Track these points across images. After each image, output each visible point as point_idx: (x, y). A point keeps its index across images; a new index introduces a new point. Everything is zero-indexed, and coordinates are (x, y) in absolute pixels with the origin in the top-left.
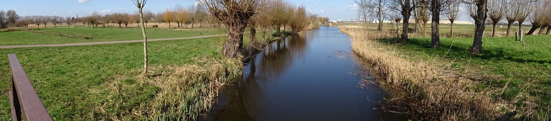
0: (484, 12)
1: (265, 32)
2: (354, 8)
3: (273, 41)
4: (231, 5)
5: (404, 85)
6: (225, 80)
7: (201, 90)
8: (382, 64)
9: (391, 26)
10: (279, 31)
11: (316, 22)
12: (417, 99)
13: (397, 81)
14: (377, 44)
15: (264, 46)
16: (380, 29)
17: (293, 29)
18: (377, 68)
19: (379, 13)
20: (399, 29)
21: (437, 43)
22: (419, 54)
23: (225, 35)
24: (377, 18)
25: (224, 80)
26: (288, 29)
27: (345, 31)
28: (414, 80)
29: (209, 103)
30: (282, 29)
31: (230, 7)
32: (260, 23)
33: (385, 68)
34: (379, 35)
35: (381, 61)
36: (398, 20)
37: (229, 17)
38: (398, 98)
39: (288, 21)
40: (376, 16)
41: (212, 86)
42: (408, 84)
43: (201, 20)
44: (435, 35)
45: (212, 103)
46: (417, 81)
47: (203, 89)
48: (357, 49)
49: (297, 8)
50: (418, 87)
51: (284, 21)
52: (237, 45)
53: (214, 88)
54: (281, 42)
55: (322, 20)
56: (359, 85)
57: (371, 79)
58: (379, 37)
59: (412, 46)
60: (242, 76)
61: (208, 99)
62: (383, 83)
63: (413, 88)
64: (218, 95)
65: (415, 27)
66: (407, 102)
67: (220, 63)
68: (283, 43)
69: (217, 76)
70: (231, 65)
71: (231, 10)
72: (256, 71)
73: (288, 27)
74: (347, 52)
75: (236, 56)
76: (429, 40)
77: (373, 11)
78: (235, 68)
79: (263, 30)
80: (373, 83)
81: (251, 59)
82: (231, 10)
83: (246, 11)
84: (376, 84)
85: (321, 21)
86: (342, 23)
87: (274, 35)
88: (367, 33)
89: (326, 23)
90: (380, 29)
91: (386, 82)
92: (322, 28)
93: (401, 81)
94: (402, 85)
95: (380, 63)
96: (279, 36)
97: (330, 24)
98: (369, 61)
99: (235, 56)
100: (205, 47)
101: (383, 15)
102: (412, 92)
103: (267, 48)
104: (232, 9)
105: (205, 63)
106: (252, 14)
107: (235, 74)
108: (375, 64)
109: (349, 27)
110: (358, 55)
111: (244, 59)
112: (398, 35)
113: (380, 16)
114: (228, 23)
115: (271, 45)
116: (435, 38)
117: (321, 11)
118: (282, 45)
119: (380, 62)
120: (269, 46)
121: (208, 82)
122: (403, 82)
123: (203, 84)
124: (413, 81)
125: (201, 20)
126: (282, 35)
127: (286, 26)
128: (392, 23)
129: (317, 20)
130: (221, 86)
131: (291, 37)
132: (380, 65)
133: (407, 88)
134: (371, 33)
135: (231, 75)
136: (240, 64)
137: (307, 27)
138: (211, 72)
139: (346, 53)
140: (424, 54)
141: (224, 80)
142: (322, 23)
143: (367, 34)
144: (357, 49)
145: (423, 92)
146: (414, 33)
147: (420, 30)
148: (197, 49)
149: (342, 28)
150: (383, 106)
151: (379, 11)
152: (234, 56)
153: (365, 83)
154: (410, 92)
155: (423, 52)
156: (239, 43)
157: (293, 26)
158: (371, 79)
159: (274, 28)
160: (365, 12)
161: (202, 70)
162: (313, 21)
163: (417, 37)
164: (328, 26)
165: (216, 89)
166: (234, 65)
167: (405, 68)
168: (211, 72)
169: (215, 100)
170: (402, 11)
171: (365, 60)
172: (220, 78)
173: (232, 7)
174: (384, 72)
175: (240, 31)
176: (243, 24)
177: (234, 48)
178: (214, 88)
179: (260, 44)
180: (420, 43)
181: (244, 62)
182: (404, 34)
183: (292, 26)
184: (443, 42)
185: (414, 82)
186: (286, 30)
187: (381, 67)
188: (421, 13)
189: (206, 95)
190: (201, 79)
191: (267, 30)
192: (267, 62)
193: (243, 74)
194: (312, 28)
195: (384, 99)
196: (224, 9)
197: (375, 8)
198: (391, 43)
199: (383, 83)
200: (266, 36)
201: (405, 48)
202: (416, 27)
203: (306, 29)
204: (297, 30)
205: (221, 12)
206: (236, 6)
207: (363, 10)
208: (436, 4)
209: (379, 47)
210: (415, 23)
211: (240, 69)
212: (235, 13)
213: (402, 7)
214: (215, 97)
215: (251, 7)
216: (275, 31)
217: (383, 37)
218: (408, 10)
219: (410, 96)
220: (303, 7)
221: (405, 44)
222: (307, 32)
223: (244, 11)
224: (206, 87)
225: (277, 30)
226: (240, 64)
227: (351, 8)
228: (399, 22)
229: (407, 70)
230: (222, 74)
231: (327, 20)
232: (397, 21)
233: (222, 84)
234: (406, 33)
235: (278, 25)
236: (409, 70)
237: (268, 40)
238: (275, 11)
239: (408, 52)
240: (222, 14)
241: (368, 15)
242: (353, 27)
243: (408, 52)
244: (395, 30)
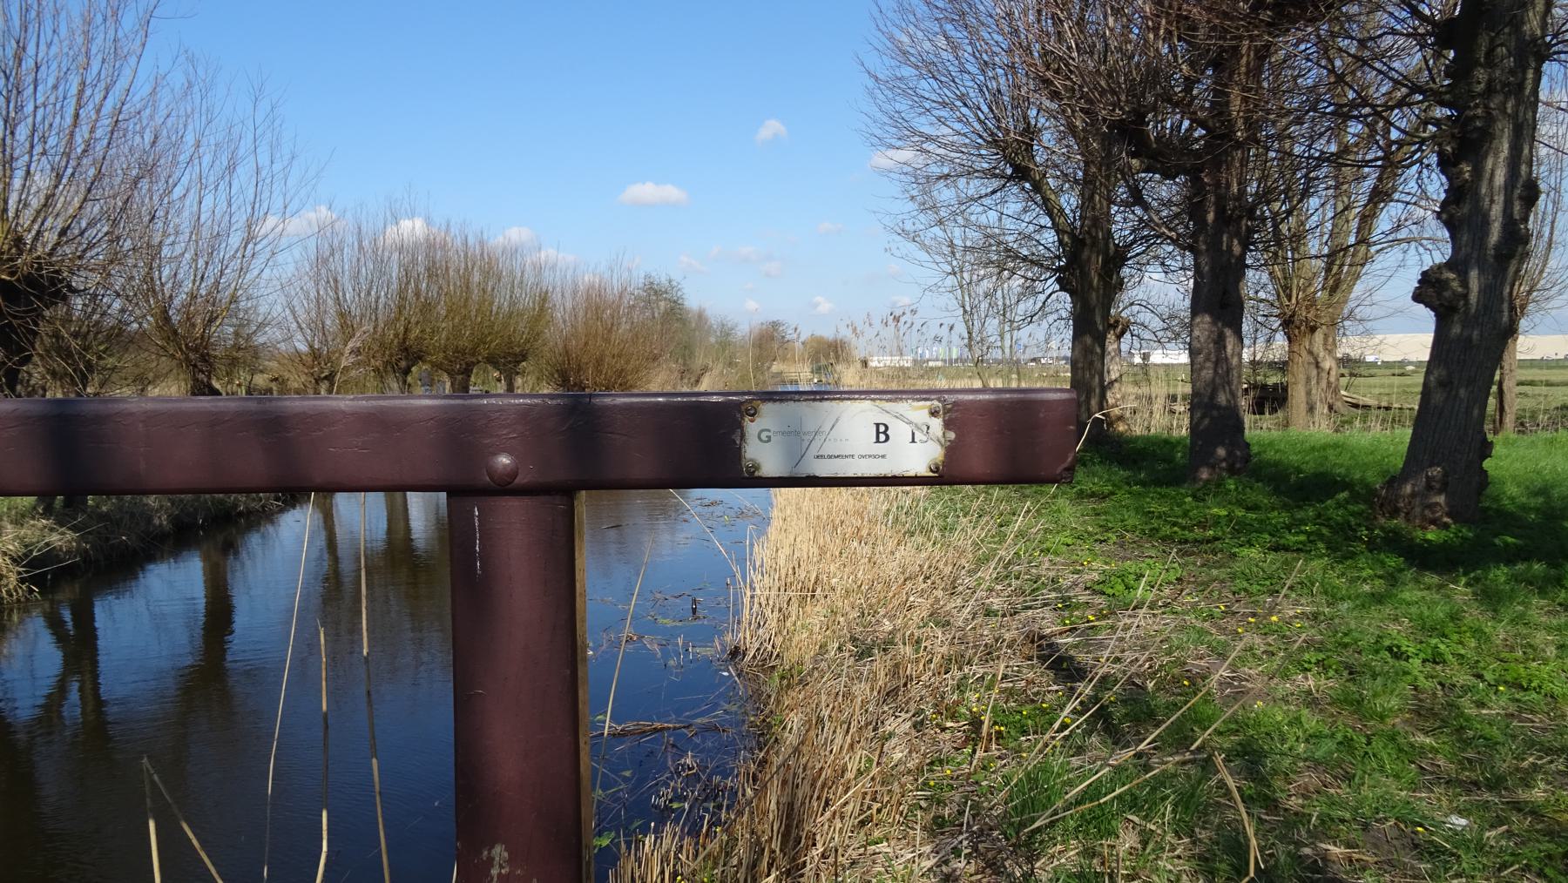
0: (1496, 211)
21: (1221, 452)
44: (1206, 400)
76: (1553, 487)
116: (1206, 421)
117: (816, 305)
195: (436, 804)
208: (1217, 204)
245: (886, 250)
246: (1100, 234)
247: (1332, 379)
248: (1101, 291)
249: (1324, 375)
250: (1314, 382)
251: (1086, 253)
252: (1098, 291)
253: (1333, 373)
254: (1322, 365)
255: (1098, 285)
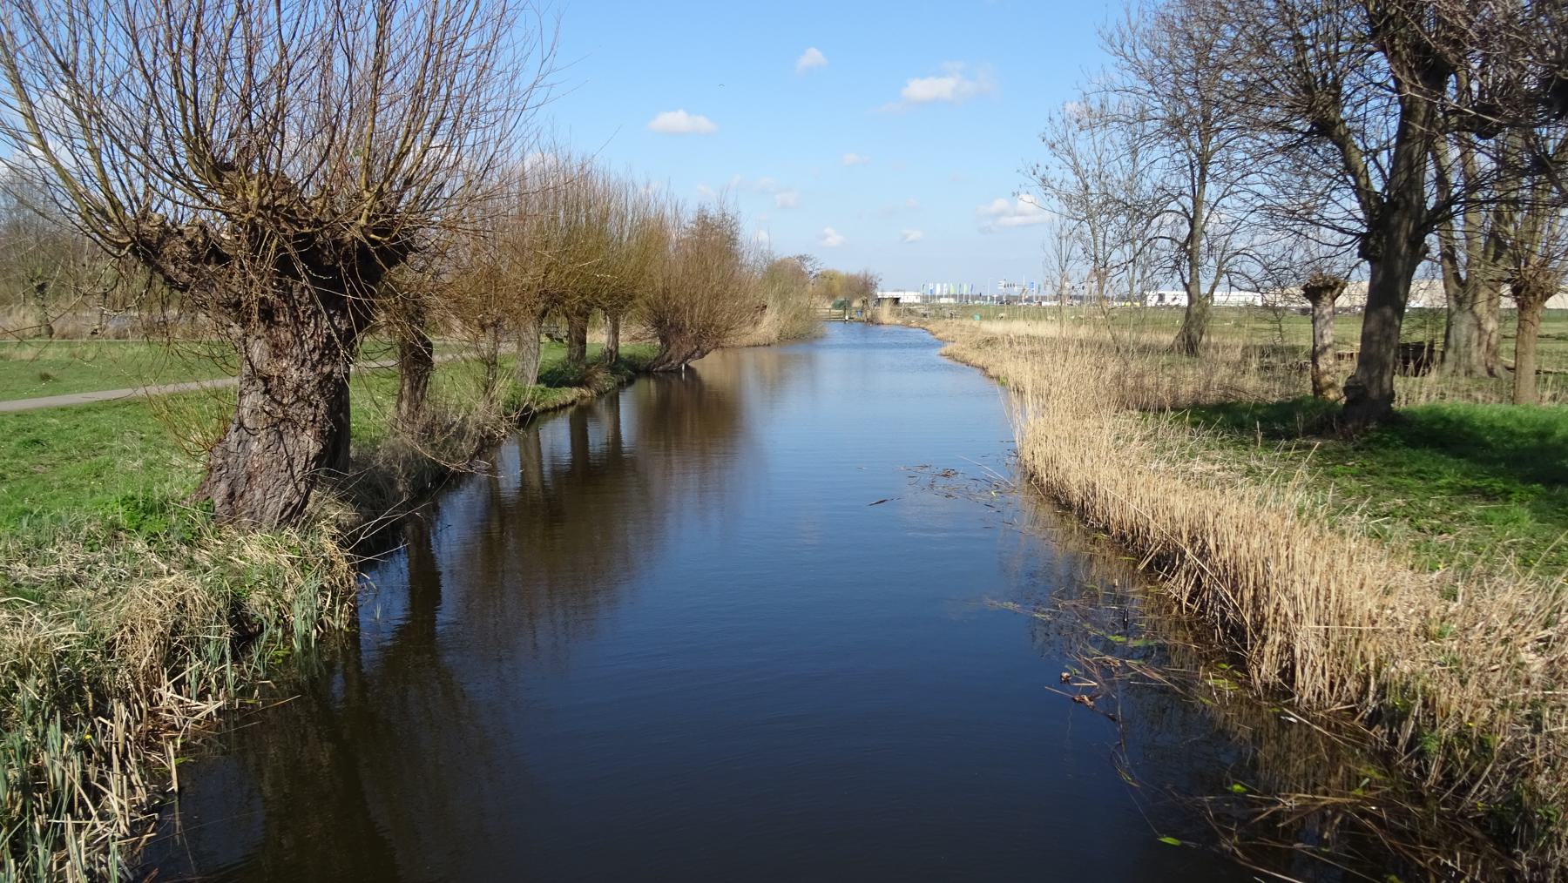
1: (491, 363)
2: (1018, 220)
3: (546, 411)
4: (252, 197)
5: (1374, 719)
6: (231, 675)
7: (39, 771)
8: (1217, 559)
9: (1266, 325)
10: (583, 351)
11: (804, 301)
12: (1477, 833)
13: (1322, 683)
14: (1177, 436)
15: (488, 444)
16: (1190, 345)
17: (664, 340)
18: (1178, 587)
19: (1188, 251)
20: (1324, 348)
22: (1483, 519)
23: (219, 383)
24: (1177, 277)
25: (221, 681)
26: (635, 339)
27: (973, 356)
28: (1449, 696)
29: (106, 852)
30: (598, 338)
31: (246, 210)
32: (459, 306)
33: (1235, 589)
34: (1190, 381)
35: (1212, 545)
36: (1320, 289)
37: (242, 267)
38: (1330, 799)
39: (631, 297)
40: (1172, 264)
41: (128, 728)
42: (1404, 716)
43: (41, 288)
45: (129, 851)
46: (1477, 706)
47: (59, 764)
48: (1051, 462)
49: (689, 217)
50: (1484, 746)
51: (610, 297)
52: (309, 443)
53: (150, 742)
54: (597, 419)
55: (837, 287)
56: (1067, 680)
57: (1145, 654)
58: (1186, 390)
59: (1425, 459)
60: (354, 638)
61: (100, 827)
62: (1224, 684)
63: (1448, 748)
64: (175, 787)
65: (1442, 332)
66: (1400, 834)
67: (190, 565)
68: (606, 420)
69: (172, 657)
70: (271, 572)
71: (254, 228)
72: (444, 597)
73: (636, 329)
74: (989, 481)
75: (300, 512)
76: (1555, 424)
77: (1151, 233)
78: (299, 590)
79: (484, 345)
80: (1157, 676)
81: (409, 528)
82: (254, 228)
83: (359, 235)
84: (1176, 682)
85: (832, 296)
86: (965, 306)
87: (551, 379)
88: (1113, 367)
89: (857, 304)
90: (1190, 345)
91: (1246, 684)
92: (835, 332)
93: (1352, 685)
94: (1354, 712)
95: (1203, 554)
96: (580, 383)
97: (885, 313)
98: (1123, 538)
99: (294, 514)
100: (73, 468)
101: (1212, 262)
102: (1434, 771)
103: (510, 458)
104: (259, 220)
105: (63, 582)
106: (398, 253)
107: (299, 627)
108: (1166, 561)
109: (996, 328)
110: (1059, 501)
111: (361, 530)
112: (1315, 382)
113: (1194, 265)
114: (238, 305)
115: (532, 437)
117: (825, 237)
118: (598, 437)
119: (1203, 548)
120: (524, 443)
121: (102, 709)
122: (1364, 692)
123: (54, 730)
124: (1444, 699)
125: (41, 288)
126: (600, 375)
127: (622, 324)
128: (1274, 309)
129: (810, 288)
130: (198, 722)
131: (653, 392)
132: (1203, 571)
133: (1393, 741)
134: (1135, 366)
135: (272, 639)
136: (332, 564)
137: (748, 329)
138: (118, 636)
139: (983, 485)
140: (1528, 522)
141: (221, 681)
142: (836, 306)
143: (1108, 376)
144: (1051, 462)
145: (1533, 792)
146: (1433, 377)
147: (1478, 356)
148: (10, 491)
149: (959, 334)
150: (1229, 834)
151: (1191, 237)
152: (290, 515)
153: (1107, 671)
154: (1418, 770)
155: (1515, 509)
156: (322, 432)
157: (665, 324)
158: (1145, 654)
159: (549, 336)
160: (1100, 239)
161: (46, 632)
162: (783, 295)
163: (1455, 404)
164: (873, 321)
165: (161, 750)
166: (290, 571)
167: (1383, 607)
168: (118, 636)
169: (158, 823)
170: (1364, 230)
171: (1098, 529)
172: (191, 669)
173: (260, 206)
174: (1230, 615)
175: (322, 355)
176: (343, 316)
177: (290, 465)
178: (150, 742)
179: (461, 433)
180: (1487, 446)
181: (362, 549)
182: (1371, 381)
183: (659, 323)
184: (1552, 413)
185: (1454, 707)
186: (626, 347)
187: (1205, 581)
188: (1496, 242)
189: (82, 803)
190: (42, 694)
191: (507, 348)
192: (511, 544)
193: (354, 622)
194: (774, 336)
195: (1237, 787)
196: (204, 215)
197: (1169, 219)
198: (1271, 436)
199: (1218, 683)
200: (500, 384)
201: (1370, 473)
202: (1447, 336)
203: (745, 341)
204: (687, 349)
205: (180, 233)
206: (284, 201)
207: (1087, 228)
209: (1192, 454)
210: (1441, 303)
211: (334, 595)
212: (280, 249)
213: (1364, 206)
214: (158, 806)
215: (393, 211)
216: (554, 355)
217: (1213, 397)
218: (1408, 226)
219: (1420, 799)
220: (724, 215)
221: (1368, 447)
222: (748, 357)
223: (348, 237)
224: (83, 747)
225: (570, 346)
226: (332, 564)
227: (1005, 220)
228: (1327, 299)
229: (1394, 621)
230: (208, 641)
231: (863, 288)
232: (1314, 292)
233: (211, 707)
234: (1381, 374)
235: (576, 319)
236: (1416, 621)
237: (511, 404)
238: (557, 238)
239: (1400, 501)
240: (184, 248)
241: (1116, 256)
242: (1020, 327)
243: (1400, 501)
244: (1294, 350)
245: (1014, 194)
246: (1415, 198)
247: (1493, 341)
248: (1408, 260)
249: (1486, 337)
250: (1474, 344)
251: (1395, 219)
252: (1404, 260)
253: (1494, 335)
254: (1484, 326)
255: (1405, 253)
